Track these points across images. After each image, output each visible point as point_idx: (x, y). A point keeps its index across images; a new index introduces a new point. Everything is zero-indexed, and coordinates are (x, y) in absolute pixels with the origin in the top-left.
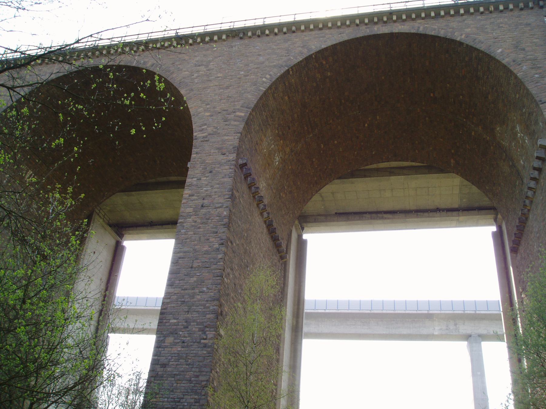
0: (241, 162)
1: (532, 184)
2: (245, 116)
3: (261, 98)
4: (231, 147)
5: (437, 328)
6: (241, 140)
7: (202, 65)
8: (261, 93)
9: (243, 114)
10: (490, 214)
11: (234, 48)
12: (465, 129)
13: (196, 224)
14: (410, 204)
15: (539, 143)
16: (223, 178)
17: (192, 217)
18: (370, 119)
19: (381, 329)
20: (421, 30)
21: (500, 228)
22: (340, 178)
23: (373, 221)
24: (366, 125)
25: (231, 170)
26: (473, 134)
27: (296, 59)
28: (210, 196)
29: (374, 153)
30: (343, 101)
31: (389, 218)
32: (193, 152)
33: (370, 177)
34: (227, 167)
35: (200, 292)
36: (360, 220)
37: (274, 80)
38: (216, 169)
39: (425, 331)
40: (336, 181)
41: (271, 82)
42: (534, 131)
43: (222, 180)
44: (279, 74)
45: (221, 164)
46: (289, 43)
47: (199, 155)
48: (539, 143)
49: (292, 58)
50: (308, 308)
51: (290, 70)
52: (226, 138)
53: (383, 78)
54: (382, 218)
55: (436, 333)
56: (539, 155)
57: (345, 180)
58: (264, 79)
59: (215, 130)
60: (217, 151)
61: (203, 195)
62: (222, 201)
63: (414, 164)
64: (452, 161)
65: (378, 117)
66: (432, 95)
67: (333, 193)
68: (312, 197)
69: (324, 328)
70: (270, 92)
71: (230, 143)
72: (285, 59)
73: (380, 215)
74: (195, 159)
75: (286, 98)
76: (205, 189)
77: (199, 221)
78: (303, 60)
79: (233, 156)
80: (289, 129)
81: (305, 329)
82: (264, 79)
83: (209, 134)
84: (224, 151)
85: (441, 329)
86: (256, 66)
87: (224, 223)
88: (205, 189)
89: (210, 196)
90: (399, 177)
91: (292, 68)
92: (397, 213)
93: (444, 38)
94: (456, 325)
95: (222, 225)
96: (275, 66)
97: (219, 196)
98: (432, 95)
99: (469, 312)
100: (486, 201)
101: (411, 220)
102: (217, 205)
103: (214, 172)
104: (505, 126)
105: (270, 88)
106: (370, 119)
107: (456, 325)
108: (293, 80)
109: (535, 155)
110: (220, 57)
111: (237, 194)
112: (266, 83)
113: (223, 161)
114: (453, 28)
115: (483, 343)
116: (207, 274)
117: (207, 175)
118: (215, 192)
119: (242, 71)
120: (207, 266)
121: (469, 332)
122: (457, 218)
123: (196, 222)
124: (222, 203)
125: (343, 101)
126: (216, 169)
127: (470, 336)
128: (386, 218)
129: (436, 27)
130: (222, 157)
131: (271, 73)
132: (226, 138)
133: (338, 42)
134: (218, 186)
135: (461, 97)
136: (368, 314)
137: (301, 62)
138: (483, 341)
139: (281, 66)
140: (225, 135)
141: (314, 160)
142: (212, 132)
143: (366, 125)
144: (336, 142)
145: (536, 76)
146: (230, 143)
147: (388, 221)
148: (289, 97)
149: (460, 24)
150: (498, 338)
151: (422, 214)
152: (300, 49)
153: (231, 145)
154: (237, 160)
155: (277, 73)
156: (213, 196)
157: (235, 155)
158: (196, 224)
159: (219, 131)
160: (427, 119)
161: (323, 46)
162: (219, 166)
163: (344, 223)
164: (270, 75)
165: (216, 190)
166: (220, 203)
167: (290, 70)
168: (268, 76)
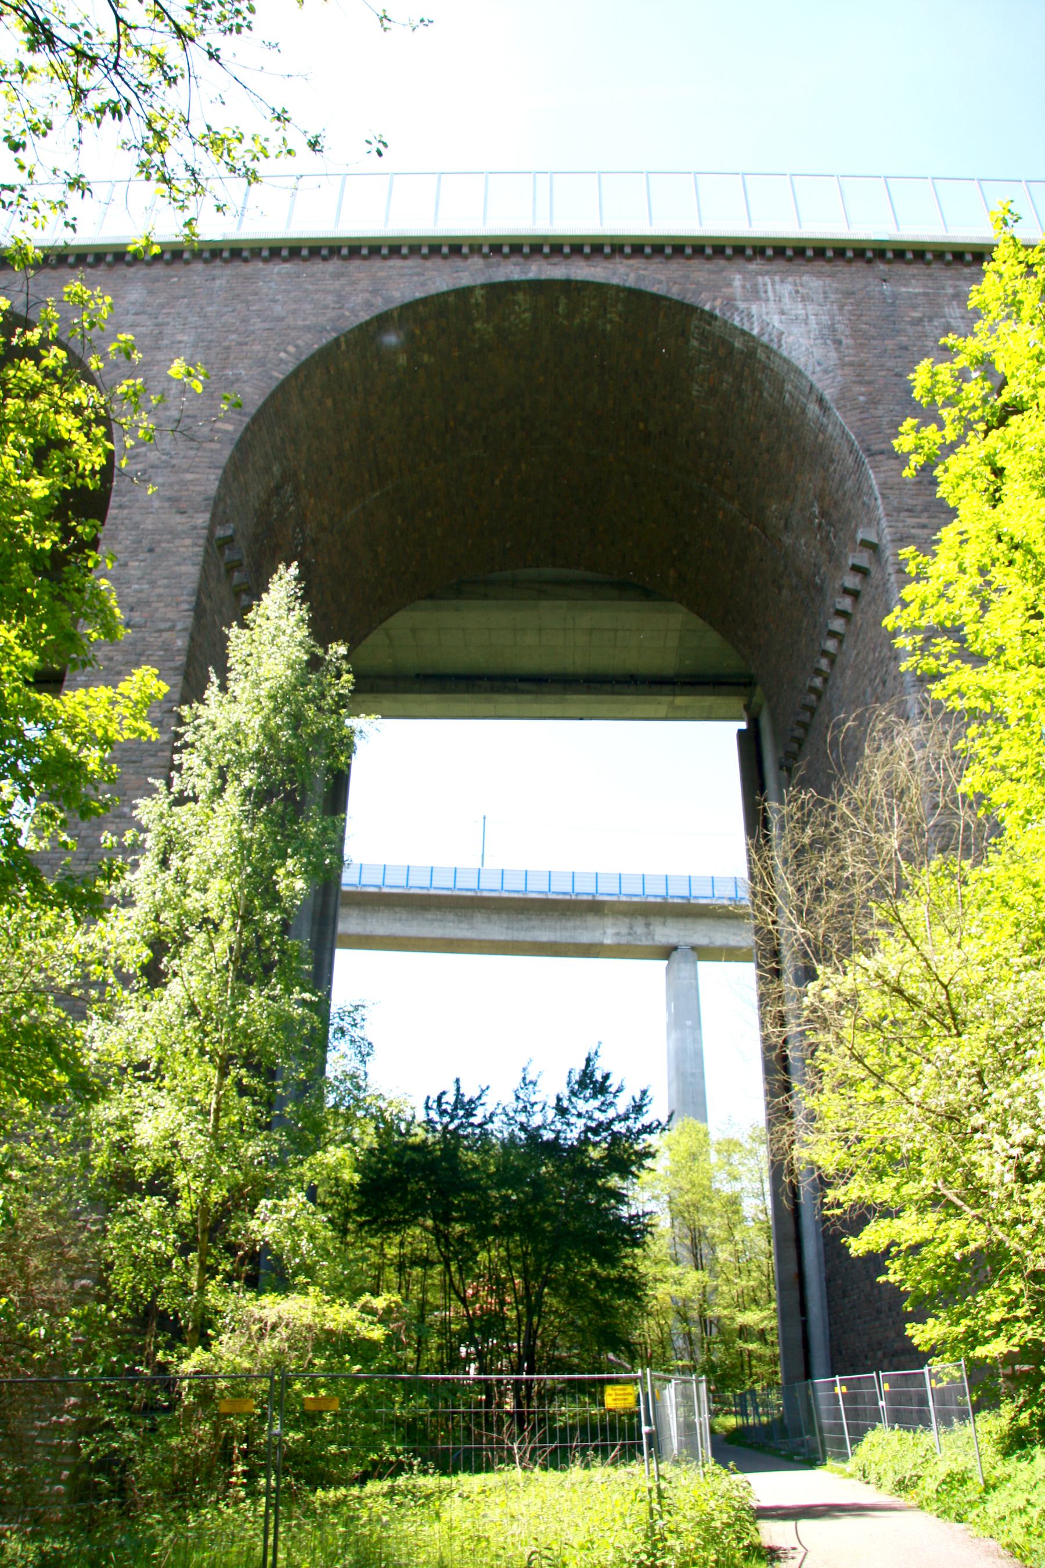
0: (220, 532)
1: (845, 603)
2: (236, 431)
3: (273, 396)
4: (199, 499)
5: (609, 933)
6: (224, 482)
7: (144, 313)
8: (274, 385)
9: (230, 428)
10: (735, 694)
11: (218, 282)
12: (705, 505)
13: (112, 664)
14: (575, 661)
15: (860, 536)
16: (178, 564)
17: (104, 649)
18: (505, 468)
19: (496, 930)
20: (631, 282)
21: (754, 723)
22: (431, 596)
23: (496, 696)
24: (497, 482)
25: (196, 549)
26: (720, 517)
27: (357, 316)
28: (148, 603)
29: (508, 545)
30: (452, 424)
31: (528, 692)
32: (112, 504)
33: (496, 598)
34: (188, 542)
35: (116, 817)
36: (467, 692)
37: (304, 358)
38: (163, 545)
39: (585, 937)
40: (423, 603)
41: (298, 363)
42: (849, 512)
43: (177, 569)
44: (316, 346)
45: (174, 534)
46: (343, 281)
47: (126, 511)
48: (860, 536)
49: (347, 314)
50: (349, 879)
51: (343, 339)
52: (189, 477)
53: (542, 379)
54: (516, 691)
55: (608, 941)
56: (858, 562)
57: (442, 602)
58: (283, 355)
59: (164, 458)
60: (167, 505)
61: (130, 600)
62: (172, 615)
63: (589, 575)
64: (672, 572)
65: (523, 466)
66: (641, 426)
67: (414, 630)
68: (369, 633)
69: (379, 925)
70: (293, 383)
71: (198, 488)
72: (331, 314)
73: (511, 685)
74: (115, 518)
75: (329, 402)
76: (135, 586)
77: (119, 657)
78: (372, 320)
79: (203, 519)
80: (331, 474)
81: (342, 927)
82: (283, 355)
83: (152, 467)
84: (183, 505)
85: (618, 934)
86: (267, 325)
87: (178, 664)
88: (135, 586)
89: (148, 603)
90: (558, 603)
91: (345, 335)
92: (546, 681)
93: (677, 302)
94: (648, 925)
95: (171, 669)
96: (308, 329)
97: (167, 606)
98: (641, 426)
99: (676, 901)
100: (730, 662)
101: (575, 697)
102: (163, 626)
103: (158, 550)
104: (788, 503)
105: (295, 374)
106: (505, 468)
107: (648, 925)
108: (346, 364)
109: (850, 562)
110: (184, 297)
111: (207, 604)
112: (286, 363)
113: (180, 528)
114: (697, 283)
115: (701, 965)
116: (133, 777)
117: (141, 557)
118: (160, 596)
119: (233, 332)
120: (134, 758)
121: (673, 940)
122: (670, 698)
123: (111, 659)
124: (174, 621)
125: (452, 424)
126: (163, 545)
127: (675, 948)
128: (522, 692)
129: (663, 278)
130: (178, 518)
131: (300, 342)
132: (189, 477)
133: (451, 287)
134: (165, 581)
135: (703, 434)
136: (471, 898)
137: (368, 323)
138: (700, 959)
139: (323, 330)
140: (187, 471)
141: (380, 549)
142: (157, 462)
143: (497, 482)
144: (429, 514)
145: (862, 398)
146: (198, 488)
147: (529, 697)
148: (335, 402)
149: (712, 277)
150: (731, 954)
151: (598, 686)
152: (367, 295)
153: (199, 493)
154: (211, 529)
155: (312, 343)
156: (154, 605)
157: (207, 516)
158: (112, 664)
159: (174, 461)
160: (627, 477)
161: (418, 295)
162: (169, 537)
163: (434, 697)
164: (297, 347)
165: (160, 591)
166: (169, 620)
167: (343, 339)
168: (291, 349)
